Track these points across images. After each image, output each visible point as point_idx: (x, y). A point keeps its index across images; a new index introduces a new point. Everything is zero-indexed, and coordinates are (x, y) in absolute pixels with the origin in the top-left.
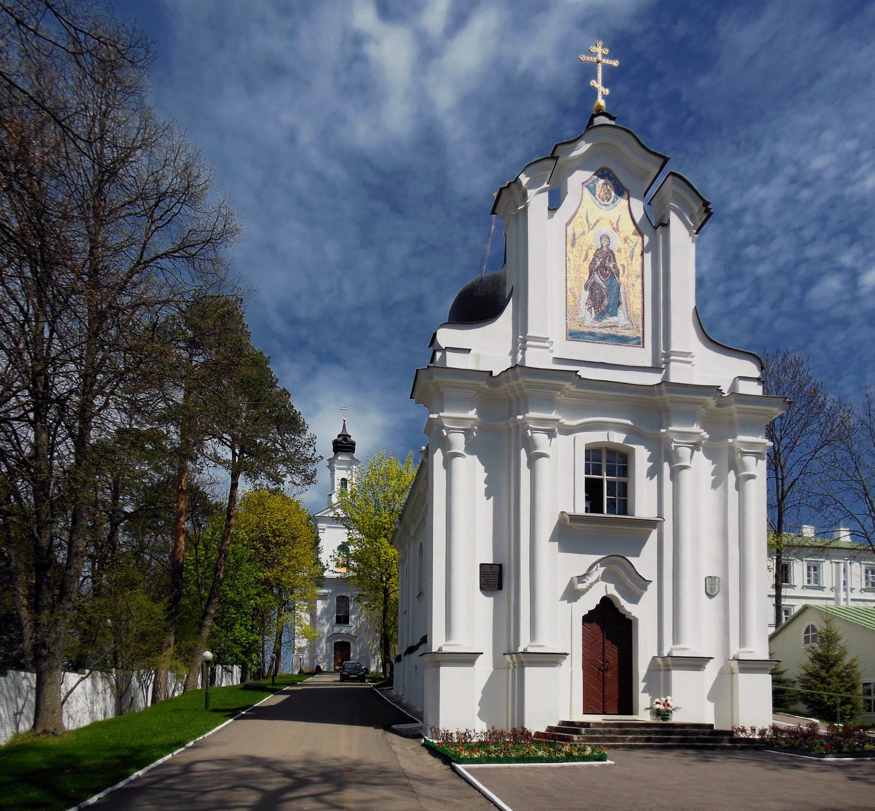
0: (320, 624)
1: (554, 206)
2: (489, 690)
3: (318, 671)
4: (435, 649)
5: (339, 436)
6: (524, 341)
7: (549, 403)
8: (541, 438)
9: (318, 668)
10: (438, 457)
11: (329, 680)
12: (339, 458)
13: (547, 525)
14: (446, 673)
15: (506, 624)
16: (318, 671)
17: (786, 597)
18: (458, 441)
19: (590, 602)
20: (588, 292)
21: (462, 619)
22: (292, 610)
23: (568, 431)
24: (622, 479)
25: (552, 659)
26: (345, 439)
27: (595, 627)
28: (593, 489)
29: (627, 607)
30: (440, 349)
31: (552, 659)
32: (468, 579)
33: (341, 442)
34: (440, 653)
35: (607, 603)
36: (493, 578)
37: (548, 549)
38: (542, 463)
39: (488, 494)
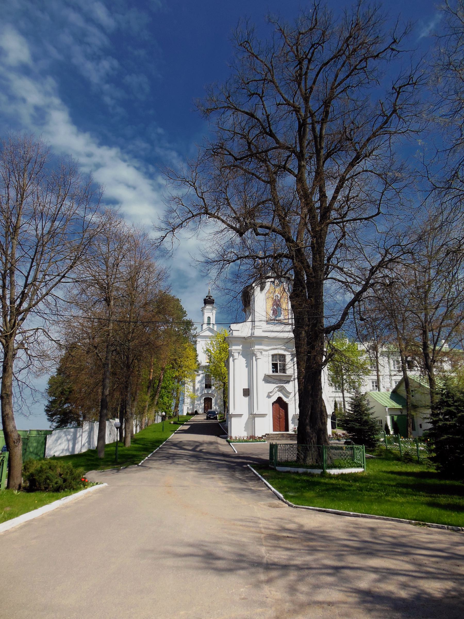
0: (160, 229)
1: (262, 289)
2: (247, 424)
3: (196, 413)
4: (230, 413)
5: (207, 297)
6: (254, 327)
7: (260, 344)
8: (258, 355)
9: (196, 412)
10: (231, 359)
11: (201, 418)
12: (207, 307)
13: (261, 377)
14: (233, 420)
15: (251, 406)
16: (196, 413)
17: (119, 446)
18: (236, 355)
19: (274, 399)
20: (272, 311)
21: (238, 404)
22: (184, 384)
23: (267, 351)
24: (284, 363)
25: (263, 416)
26: (210, 298)
27: (277, 405)
28: (275, 366)
29: (285, 399)
30: (231, 330)
31: (263, 416)
32: (240, 393)
33: (208, 300)
34: (232, 414)
35: (280, 399)
36: (247, 393)
37: (261, 383)
38: (258, 360)
39: (247, 367)
